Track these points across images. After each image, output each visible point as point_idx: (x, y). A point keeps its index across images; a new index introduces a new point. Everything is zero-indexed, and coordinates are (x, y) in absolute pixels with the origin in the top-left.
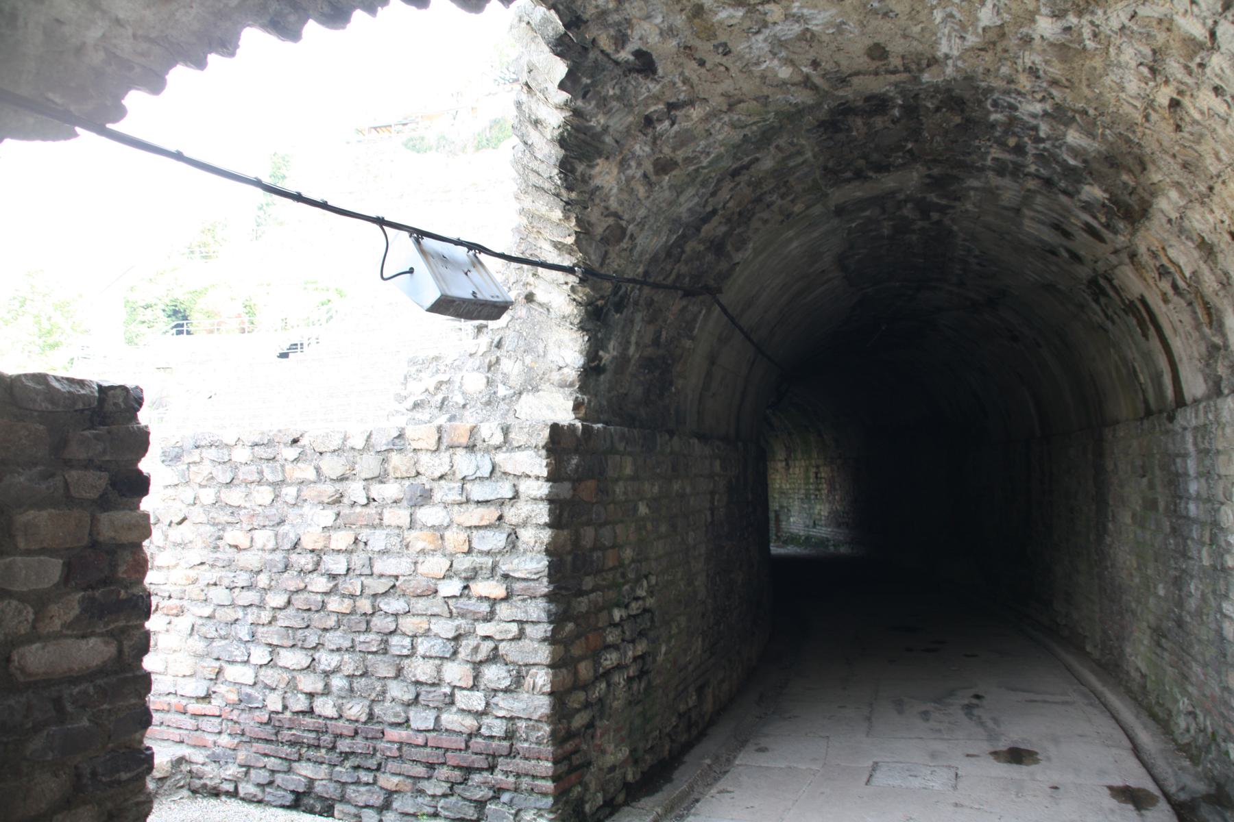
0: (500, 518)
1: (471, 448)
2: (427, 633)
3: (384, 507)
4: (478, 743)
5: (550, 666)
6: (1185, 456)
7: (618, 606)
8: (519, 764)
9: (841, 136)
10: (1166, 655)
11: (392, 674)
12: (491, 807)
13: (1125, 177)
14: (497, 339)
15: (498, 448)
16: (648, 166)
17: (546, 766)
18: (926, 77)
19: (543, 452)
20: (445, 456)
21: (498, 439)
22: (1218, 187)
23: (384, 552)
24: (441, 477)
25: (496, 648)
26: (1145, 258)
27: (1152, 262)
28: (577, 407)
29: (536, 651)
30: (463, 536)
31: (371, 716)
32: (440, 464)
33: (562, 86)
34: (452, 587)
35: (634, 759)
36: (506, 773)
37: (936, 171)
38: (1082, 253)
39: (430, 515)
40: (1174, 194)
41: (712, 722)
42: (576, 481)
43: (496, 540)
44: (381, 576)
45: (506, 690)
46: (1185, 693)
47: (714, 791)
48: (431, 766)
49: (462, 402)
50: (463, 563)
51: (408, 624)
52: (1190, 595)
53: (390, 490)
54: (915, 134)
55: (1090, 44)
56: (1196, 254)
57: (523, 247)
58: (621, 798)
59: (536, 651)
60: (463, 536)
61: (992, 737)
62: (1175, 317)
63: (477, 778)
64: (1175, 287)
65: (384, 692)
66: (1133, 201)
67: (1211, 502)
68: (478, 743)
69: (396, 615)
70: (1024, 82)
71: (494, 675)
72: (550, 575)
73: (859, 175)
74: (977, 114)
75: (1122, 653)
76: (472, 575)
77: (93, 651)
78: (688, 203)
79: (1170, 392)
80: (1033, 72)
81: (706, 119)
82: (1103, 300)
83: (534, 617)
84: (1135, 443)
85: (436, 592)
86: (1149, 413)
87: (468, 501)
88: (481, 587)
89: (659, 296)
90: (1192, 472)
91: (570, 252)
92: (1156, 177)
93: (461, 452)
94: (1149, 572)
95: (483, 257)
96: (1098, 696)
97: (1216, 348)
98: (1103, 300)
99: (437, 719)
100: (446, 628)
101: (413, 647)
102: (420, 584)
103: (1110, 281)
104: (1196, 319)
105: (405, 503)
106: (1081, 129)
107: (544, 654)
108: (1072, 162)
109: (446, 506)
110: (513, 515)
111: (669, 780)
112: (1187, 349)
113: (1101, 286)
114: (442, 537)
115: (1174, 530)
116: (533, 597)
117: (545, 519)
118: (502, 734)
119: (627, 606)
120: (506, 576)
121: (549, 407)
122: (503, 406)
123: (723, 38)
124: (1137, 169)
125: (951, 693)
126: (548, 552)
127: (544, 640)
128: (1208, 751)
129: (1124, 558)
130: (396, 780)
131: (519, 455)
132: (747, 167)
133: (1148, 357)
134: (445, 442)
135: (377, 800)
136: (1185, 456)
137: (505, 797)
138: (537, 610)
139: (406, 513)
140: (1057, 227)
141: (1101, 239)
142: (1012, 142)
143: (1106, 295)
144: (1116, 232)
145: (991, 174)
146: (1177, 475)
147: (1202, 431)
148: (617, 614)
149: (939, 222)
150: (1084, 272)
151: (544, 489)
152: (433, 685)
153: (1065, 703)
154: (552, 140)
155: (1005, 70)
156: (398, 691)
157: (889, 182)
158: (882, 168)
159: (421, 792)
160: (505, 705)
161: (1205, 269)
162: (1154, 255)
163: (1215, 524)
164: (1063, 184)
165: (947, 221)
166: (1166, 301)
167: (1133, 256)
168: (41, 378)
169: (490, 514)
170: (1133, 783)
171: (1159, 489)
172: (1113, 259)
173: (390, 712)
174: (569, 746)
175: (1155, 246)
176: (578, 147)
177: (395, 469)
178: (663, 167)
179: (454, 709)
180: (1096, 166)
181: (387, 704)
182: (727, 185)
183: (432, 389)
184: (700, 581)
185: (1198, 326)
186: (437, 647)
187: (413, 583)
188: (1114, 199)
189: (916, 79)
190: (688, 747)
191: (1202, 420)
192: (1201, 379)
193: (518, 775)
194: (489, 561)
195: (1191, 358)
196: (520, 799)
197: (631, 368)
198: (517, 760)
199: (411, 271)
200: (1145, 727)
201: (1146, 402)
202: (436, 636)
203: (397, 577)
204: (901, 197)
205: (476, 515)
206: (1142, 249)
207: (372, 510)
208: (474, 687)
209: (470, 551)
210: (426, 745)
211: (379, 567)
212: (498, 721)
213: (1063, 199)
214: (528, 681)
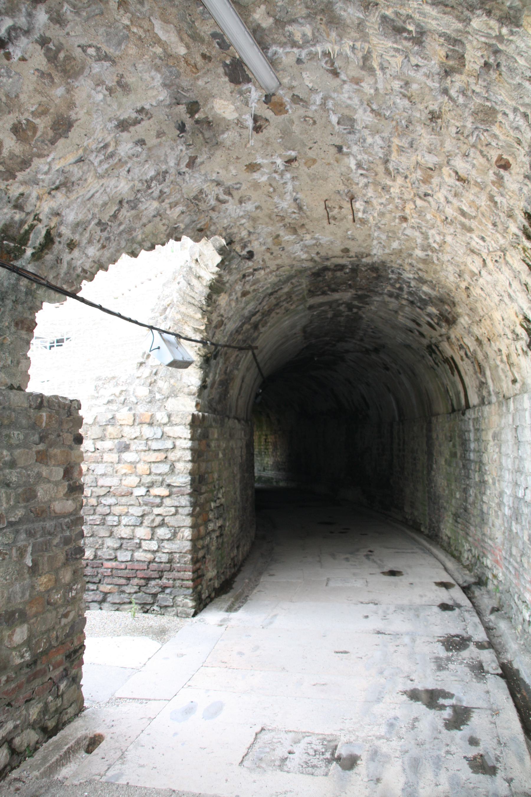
0: (166, 458)
1: (151, 424)
2: (127, 514)
3: (103, 452)
4: (154, 566)
5: (191, 527)
6: (469, 431)
7: (212, 501)
8: (175, 574)
9: (320, 279)
10: (459, 526)
11: (108, 535)
12: (160, 596)
13: (446, 307)
14: (154, 371)
15: (165, 424)
16: (239, 294)
17: (189, 574)
18: (364, 260)
19: (188, 427)
20: (137, 428)
21: (166, 420)
22: (483, 320)
23: (103, 475)
24: (135, 438)
25: (163, 520)
26: (454, 340)
27: (456, 342)
28: (197, 405)
29: (184, 520)
30: (147, 466)
31: (95, 556)
32: (134, 432)
33: (218, 266)
34: (142, 491)
35: (218, 576)
36: (168, 579)
37: (360, 293)
38: (425, 333)
39: (128, 456)
40: (466, 318)
41: (242, 565)
42: (199, 440)
43: (164, 468)
44: (102, 486)
45: (168, 540)
46: (467, 541)
47: (255, 591)
48: (128, 579)
49: (135, 401)
50: (147, 480)
51: (117, 510)
52: (470, 495)
53: (108, 444)
54: (353, 278)
55: (436, 262)
56: (475, 343)
57: (175, 328)
58: (213, 595)
59: (184, 520)
60: (147, 466)
61: (380, 567)
62: (466, 367)
63: (153, 583)
64: (466, 354)
65: (103, 544)
66: (450, 316)
67: (479, 452)
68: (154, 566)
69: (110, 506)
70: (407, 268)
71: (162, 532)
72: (191, 485)
73: (324, 293)
74: (384, 274)
75: (439, 529)
76: (152, 485)
77: (70, 505)
78: (251, 307)
79: (463, 402)
80: (411, 265)
81: (267, 274)
82: (434, 355)
83: (183, 504)
84: (447, 425)
85: (132, 493)
86: (453, 410)
87: (149, 450)
88: (156, 491)
89: (230, 351)
90: (472, 439)
91: (201, 332)
92: (460, 310)
93: (145, 427)
94: (453, 487)
95: (182, 340)
96: (429, 550)
97: (483, 383)
98: (434, 355)
99: (132, 555)
100: (137, 511)
101: (119, 521)
102: (124, 490)
103: (437, 347)
104: (475, 369)
105: (115, 450)
106: (429, 286)
107: (188, 521)
108: (424, 297)
109: (137, 451)
110: (172, 456)
111: (232, 588)
112: (471, 382)
113: (432, 349)
114: (135, 467)
115: (464, 466)
116: (183, 495)
117: (189, 458)
118: (166, 561)
119: (215, 501)
120: (169, 485)
121: (183, 405)
122: (159, 404)
123: (283, 245)
124: (452, 305)
125: (358, 550)
126: (190, 474)
127: (188, 515)
128: (476, 565)
129: (441, 481)
130: (109, 587)
131: (176, 428)
132: (276, 292)
133: (453, 384)
134: (137, 421)
135: (99, 597)
136: (469, 431)
137: (168, 591)
138: (185, 501)
139: (117, 455)
140: (414, 321)
141: (434, 329)
142: (398, 285)
143: (435, 353)
144: (441, 327)
145: (385, 296)
146: (466, 440)
147: (476, 420)
148: (213, 505)
149: (356, 313)
150: (425, 342)
151: (189, 444)
152: (130, 539)
153: (413, 553)
154: (206, 286)
155: (399, 262)
156: (111, 543)
157: (336, 296)
158: (334, 290)
159: (123, 592)
160: (168, 547)
161: (478, 350)
162: (458, 340)
163: (481, 462)
164: (419, 304)
165: (360, 313)
166: (462, 360)
167: (448, 338)
168: (56, 397)
169: (161, 456)
170: (444, 580)
171: (458, 447)
172: (440, 339)
173: (107, 554)
174: (198, 565)
175: (458, 336)
176: (216, 288)
177: (110, 434)
178: (244, 294)
179: (141, 550)
180: (434, 300)
181: (105, 550)
182: (267, 299)
183: (117, 394)
184: (238, 493)
185: (475, 373)
186: (132, 521)
187: (120, 490)
188: (441, 314)
189: (359, 260)
190: (234, 575)
191: (476, 416)
192: (476, 396)
193: (174, 580)
194: (160, 478)
195: (472, 387)
196: (175, 591)
197: (216, 386)
198: (174, 572)
199: (159, 348)
200: (450, 560)
201: (452, 405)
202: (132, 515)
203: (110, 487)
204: (341, 302)
205: (153, 457)
206: (453, 336)
207: (97, 454)
208: (152, 539)
209: (150, 474)
210: (126, 569)
211: (101, 482)
212: (164, 555)
213: (418, 310)
214: (180, 535)
